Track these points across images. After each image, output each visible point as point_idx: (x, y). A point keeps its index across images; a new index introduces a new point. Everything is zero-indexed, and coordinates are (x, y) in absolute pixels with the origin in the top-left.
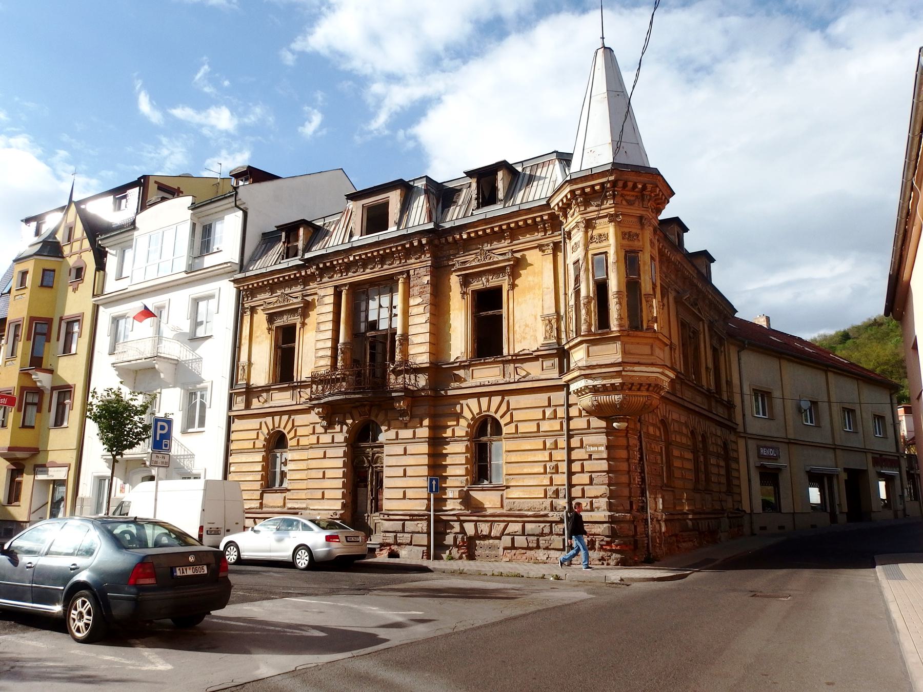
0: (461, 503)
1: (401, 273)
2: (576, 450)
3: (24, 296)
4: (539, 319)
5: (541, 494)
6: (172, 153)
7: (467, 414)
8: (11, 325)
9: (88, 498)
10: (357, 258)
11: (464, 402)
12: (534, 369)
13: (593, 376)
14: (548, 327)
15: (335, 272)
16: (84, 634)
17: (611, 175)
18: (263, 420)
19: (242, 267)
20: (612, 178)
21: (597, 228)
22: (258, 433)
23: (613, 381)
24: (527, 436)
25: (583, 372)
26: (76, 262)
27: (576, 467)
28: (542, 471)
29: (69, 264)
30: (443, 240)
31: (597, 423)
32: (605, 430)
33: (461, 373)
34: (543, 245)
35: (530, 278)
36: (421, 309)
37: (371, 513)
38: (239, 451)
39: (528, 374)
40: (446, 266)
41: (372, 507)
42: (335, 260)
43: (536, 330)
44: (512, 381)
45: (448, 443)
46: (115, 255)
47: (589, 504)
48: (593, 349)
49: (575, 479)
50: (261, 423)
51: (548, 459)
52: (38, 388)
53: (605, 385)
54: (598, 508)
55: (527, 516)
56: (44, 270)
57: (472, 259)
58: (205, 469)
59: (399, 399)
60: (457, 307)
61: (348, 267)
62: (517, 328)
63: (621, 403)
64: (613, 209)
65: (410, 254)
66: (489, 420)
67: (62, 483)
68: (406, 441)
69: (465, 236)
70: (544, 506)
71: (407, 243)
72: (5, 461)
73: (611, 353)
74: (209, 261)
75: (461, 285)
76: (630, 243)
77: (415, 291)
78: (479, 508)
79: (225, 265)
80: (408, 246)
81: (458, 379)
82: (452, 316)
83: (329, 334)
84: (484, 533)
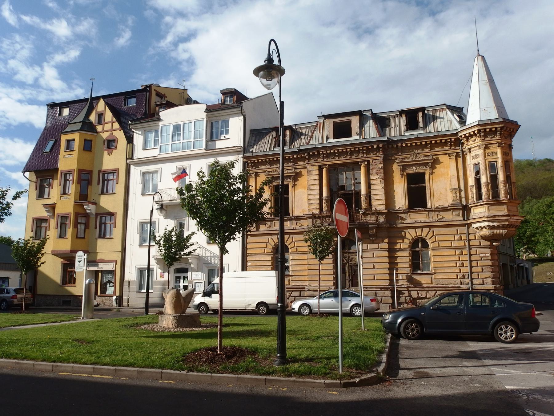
0: (407, 281)
1: (364, 161)
2: (473, 256)
3: (73, 155)
4: (449, 191)
5: (455, 277)
6: (23, 48)
7: (408, 236)
8: (63, 173)
9: (133, 281)
10: (336, 151)
11: (406, 231)
12: (448, 216)
13: (492, 221)
14: (455, 195)
15: (320, 158)
16: (515, 334)
17: (502, 124)
18: (270, 237)
19: (245, 149)
20: (502, 125)
21: (491, 149)
22: (267, 244)
23: (504, 223)
24: (444, 248)
25: (489, 219)
26: (108, 137)
27: (474, 264)
28: (455, 265)
29: (102, 138)
30: (390, 146)
31: (484, 242)
32: (489, 246)
33: (403, 215)
34: (450, 154)
35: (442, 170)
36: (378, 182)
37: (349, 287)
38: (254, 254)
39: (443, 218)
40: (390, 160)
41: (349, 284)
42: (321, 151)
43: (447, 196)
44: (434, 221)
45: (397, 251)
46: (141, 135)
47: (482, 281)
48: (491, 207)
49: (474, 269)
50: (269, 239)
51: (458, 260)
52: (87, 214)
53: (494, 225)
54: (486, 283)
55: (449, 287)
56: (85, 140)
57: (409, 158)
58: (228, 264)
59: (373, 228)
60: (398, 181)
61: (328, 156)
62: (435, 194)
63: (505, 234)
64: (500, 140)
65: (369, 152)
66: (420, 240)
67: (112, 272)
68: (373, 250)
69: (404, 145)
70: (457, 282)
71: (370, 146)
72: (59, 259)
73: (502, 210)
74: (219, 144)
75: (401, 171)
76: (506, 157)
77: (373, 171)
78: (420, 284)
79: (237, 148)
80: (370, 147)
81: (402, 219)
82: (395, 186)
83: (317, 192)
84: (423, 296)
